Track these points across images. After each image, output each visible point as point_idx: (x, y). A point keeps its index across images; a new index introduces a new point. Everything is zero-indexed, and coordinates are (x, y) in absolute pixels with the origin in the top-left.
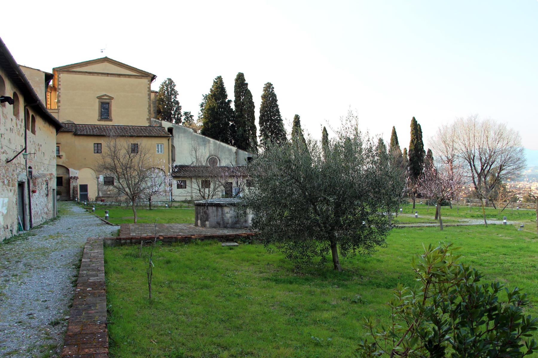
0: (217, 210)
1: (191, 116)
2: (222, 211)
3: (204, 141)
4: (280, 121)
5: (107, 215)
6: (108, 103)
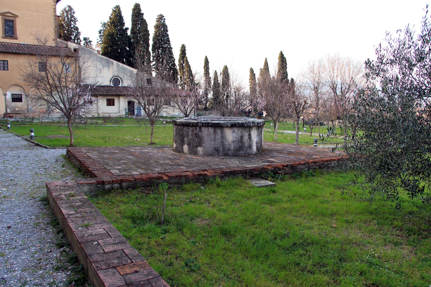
0: (215, 133)
1: (90, 42)
2: (222, 133)
3: (108, 62)
4: (170, 49)
5: (33, 134)
6: (13, 21)
